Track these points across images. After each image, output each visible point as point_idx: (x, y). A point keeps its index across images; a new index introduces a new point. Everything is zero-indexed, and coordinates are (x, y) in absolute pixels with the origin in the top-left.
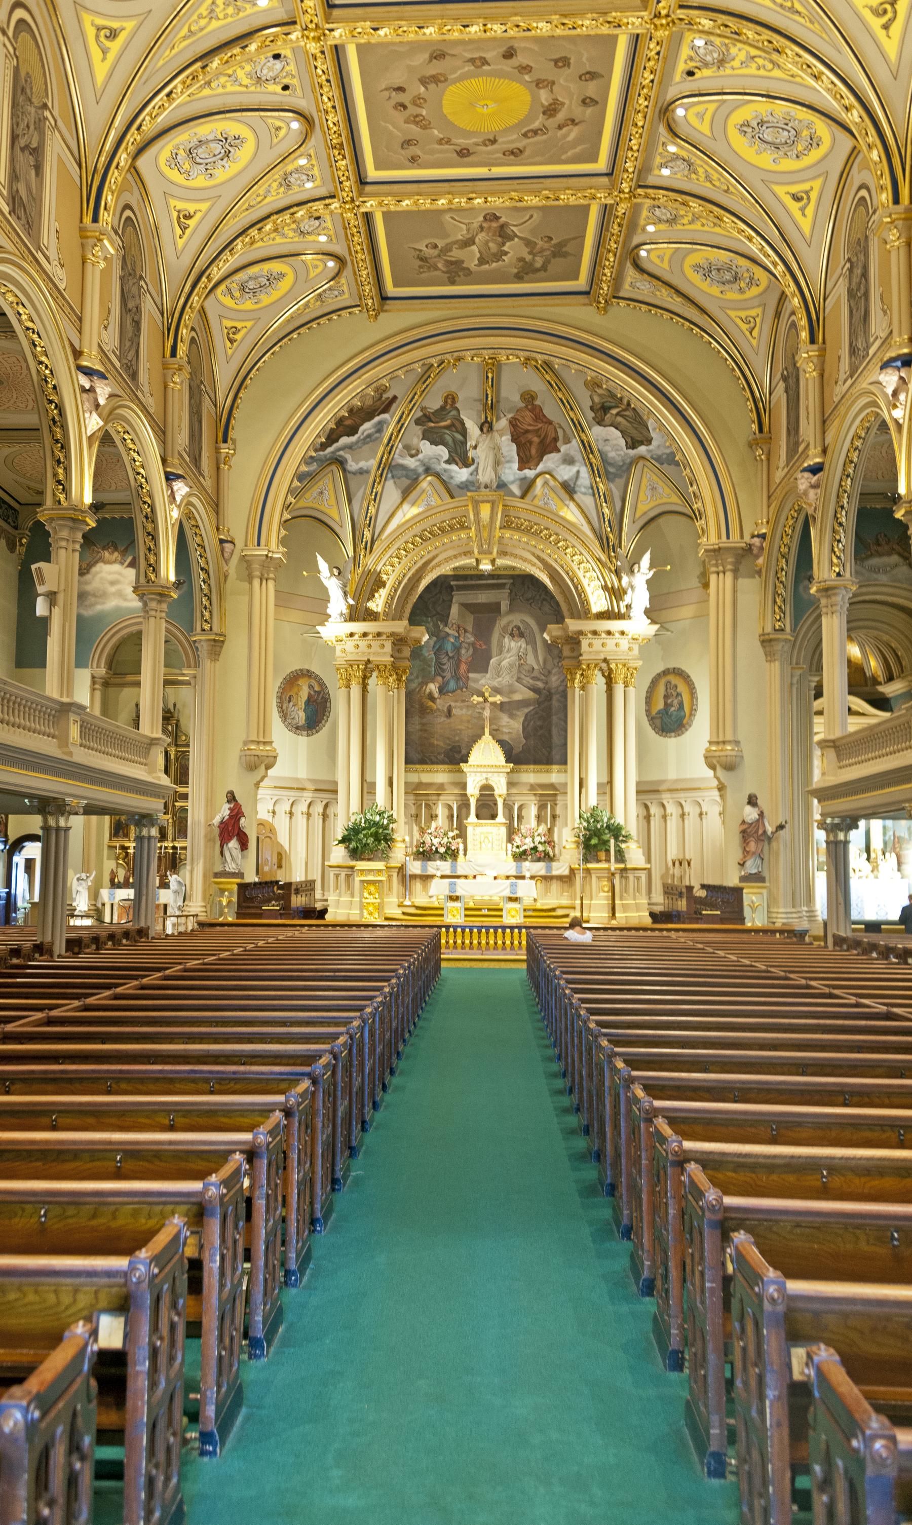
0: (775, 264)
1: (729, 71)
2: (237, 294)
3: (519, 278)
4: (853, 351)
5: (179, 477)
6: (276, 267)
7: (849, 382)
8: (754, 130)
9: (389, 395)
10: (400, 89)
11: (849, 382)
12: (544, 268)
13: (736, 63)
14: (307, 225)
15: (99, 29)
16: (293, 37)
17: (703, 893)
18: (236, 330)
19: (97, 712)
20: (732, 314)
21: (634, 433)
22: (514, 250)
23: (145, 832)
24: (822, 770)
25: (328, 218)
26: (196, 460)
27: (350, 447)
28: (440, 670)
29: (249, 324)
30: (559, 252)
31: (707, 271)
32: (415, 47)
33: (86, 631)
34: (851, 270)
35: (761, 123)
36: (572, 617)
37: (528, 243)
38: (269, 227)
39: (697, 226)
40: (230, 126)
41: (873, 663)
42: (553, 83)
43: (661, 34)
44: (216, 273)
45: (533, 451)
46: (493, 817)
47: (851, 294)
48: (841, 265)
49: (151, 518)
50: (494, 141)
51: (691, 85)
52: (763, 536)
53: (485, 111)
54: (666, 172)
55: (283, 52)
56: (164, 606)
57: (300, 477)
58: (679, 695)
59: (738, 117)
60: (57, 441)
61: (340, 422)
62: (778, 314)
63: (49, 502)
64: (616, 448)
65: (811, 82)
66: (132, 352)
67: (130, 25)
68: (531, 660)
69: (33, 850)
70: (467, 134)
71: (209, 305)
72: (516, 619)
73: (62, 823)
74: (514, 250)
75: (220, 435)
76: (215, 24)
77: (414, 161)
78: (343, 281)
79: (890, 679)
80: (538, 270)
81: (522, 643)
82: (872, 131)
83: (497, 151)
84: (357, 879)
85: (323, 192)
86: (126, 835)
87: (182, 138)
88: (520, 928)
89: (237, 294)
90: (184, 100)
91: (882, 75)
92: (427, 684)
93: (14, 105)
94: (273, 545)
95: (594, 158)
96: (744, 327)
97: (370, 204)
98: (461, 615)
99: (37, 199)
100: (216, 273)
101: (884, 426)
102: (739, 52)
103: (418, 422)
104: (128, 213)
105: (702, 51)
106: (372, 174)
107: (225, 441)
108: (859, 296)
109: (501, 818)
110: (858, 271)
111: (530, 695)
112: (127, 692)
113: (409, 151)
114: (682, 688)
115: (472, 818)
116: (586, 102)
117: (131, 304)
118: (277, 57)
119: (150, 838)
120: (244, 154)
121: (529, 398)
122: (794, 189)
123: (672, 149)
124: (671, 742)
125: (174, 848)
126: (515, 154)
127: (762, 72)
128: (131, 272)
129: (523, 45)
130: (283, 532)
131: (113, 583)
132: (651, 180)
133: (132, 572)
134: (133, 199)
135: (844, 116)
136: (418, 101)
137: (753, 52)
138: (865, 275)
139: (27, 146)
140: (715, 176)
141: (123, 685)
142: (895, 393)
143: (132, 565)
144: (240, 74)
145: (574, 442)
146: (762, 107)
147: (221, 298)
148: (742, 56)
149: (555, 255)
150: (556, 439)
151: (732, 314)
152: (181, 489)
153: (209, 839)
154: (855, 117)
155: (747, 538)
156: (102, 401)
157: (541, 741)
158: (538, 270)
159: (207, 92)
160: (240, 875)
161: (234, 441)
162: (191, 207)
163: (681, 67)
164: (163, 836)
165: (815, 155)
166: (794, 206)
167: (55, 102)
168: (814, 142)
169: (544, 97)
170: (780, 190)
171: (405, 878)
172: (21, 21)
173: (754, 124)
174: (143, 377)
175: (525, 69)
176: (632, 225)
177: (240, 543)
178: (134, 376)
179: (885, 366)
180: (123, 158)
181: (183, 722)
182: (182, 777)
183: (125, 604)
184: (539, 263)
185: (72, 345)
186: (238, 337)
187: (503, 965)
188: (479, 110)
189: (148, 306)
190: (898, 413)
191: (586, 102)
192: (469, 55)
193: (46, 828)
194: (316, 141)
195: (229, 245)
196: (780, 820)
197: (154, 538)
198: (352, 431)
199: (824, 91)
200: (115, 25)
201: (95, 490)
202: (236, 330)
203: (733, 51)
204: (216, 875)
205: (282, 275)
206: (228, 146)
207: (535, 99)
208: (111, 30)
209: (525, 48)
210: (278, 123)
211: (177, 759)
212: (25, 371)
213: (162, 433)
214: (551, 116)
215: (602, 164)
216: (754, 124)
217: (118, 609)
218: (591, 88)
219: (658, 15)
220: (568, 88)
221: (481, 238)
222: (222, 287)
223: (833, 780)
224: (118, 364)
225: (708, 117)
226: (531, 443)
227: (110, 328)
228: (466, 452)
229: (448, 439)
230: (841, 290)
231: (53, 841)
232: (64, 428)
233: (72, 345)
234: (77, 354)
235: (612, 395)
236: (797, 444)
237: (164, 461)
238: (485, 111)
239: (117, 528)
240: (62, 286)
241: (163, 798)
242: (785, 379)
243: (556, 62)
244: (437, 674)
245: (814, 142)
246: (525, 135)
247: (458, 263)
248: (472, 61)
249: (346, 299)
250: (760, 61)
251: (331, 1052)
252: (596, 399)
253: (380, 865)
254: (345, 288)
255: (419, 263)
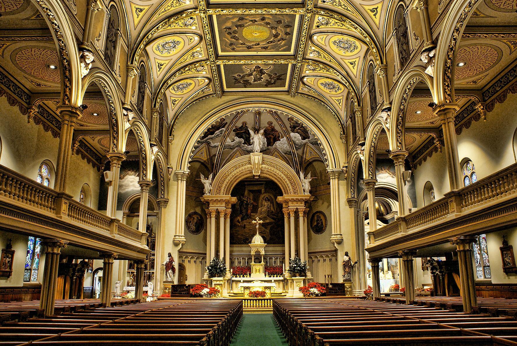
0: (346, 83)
1: (329, 26)
2: (176, 89)
3: (266, 86)
4: (372, 108)
5: (155, 145)
6: (189, 81)
7: (371, 117)
8: (337, 43)
9: (225, 122)
10: (230, 28)
11: (371, 117)
12: (274, 83)
13: (332, 24)
14: (200, 68)
15: (137, 9)
16: (197, 12)
17: (330, 286)
18: (176, 101)
19: (125, 223)
20: (334, 98)
21: (304, 135)
22: (264, 77)
23: (139, 266)
24: (369, 243)
25: (206, 66)
26: (161, 141)
27: (212, 138)
28: (241, 212)
29: (180, 99)
30: (279, 78)
31: (325, 85)
32: (235, 16)
33: (121, 200)
34: (369, 84)
35: (340, 42)
36: (285, 193)
37: (269, 75)
38: (187, 69)
39: (322, 71)
40: (176, 38)
41: (382, 208)
42: (277, 28)
43: (309, 15)
44: (170, 82)
45: (272, 141)
46: (260, 262)
47: (370, 91)
48: (366, 83)
49: (145, 158)
50: (259, 44)
51: (318, 30)
52: (346, 167)
53: (256, 35)
54: (311, 55)
55: (193, 17)
56: (148, 188)
57: (196, 148)
58: (321, 220)
59: (333, 40)
60: (115, 131)
61: (209, 130)
62: (347, 99)
63: (111, 151)
64: (298, 140)
65: (354, 30)
66: (141, 105)
67: (146, 8)
68: (272, 208)
69: (100, 274)
70: (249, 42)
71: (167, 92)
72: (267, 195)
73: (111, 261)
74: (264, 77)
75: (169, 133)
76: (173, 8)
77: (233, 50)
78: (210, 86)
79: (388, 213)
80: (273, 84)
81: (269, 203)
82: (373, 43)
83: (260, 47)
84: (213, 283)
85: (205, 58)
86: (133, 268)
87: (160, 41)
88: (270, 299)
89: (176, 89)
90: (161, 31)
91: (375, 28)
92: (237, 217)
93: (108, 28)
94: (186, 170)
95: (289, 50)
96: (337, 102)
97: (219, 62)
98: (249, 194)
99: (113, 56)
100: (170, 82)
101: (383, 131)
102: (332, 21)
103: (234, 131)
104: (142, 63)
105: (321, 21)
106: (220, 53)
107: (170, 135)
108: (372, 91)
109: (262, 263)
110: (372, 84)
111: (272, 220)
112: (135, 218)
113: (232, 46)
114: (322, 217)
115: (253, 263)
116: (287, 34)
117: (142, 90)
118: (191, 18)
119: (141, 268)
120: (179, 47)
121: (270, 123)
122: (350, 61)
123: (313, 48)
124: (319, 236)
125: (150, 273)
126: (265, 48)
127: (339, 27)
128: (143, 79)
129: (267, 16)
130: (189, 165)
131: (131, 182)
132: (307, 57)
133: (138, 178)
134: (145, 59)
135: (365, 40)
136: (235, 32)
137: (337, 21)
138: (374, 85)
139: (111, 40)
140: (327, 57)
141: (133, 217)
142: (386, 120)
143: (139, 175)
144: (180, 23)
145: (285, 138)
146: (340, 37)
147: (171, 91)
148: (333, 22)
149: (278, 79)
150: (279, 137)
151: (334, 98)
152: (155, 149)
153: (162, 269)
154: (368, 39)
155: (341, 167)
156: (130, 119)
157: (275, 235)
158: (273, 84)
159: (169, 28)
160: (173, 282)
161: (174, 136)
162: (162, 62)
163: (315, 24)
164: (146, 269)
165: (356, 51)
166: (351, 66)
167: (121, 29)
168: (356, 47)
169: (274, 32)
170: (346, 61)
171: (230, 282)
172: (112, 5)
173: (338, 42)
174: (145, 113)
175: (268, 24)
176: (301, 70)
177: (174, 168)
178: (141, 112)
179: (383, 111)
180: (142, 46)
181: (154, 229)
182: (153, 247)
183: (135, 189)
184: (273, 81)
185: (121, 101)
186: (176, 103)
187: (264, 313)
188: (254, 35)
189: (148, 91)
190: (388, 125)
191: (287, 34)
192: (251, 19)
193: (105, 263)
194: (203, 43)
195: (174, 74)
196: (356, 260)
197: (146, 165)
198: (212, 133)
199: (357, 32)
200: (142, 8)
201: (127, 145)
202: (176, 101)
203: (331, 21)
204: (164, 282)
205: (191, 84)
206: (175, 44)
207: (271, 32)
208: (141, 9)
209: (268, 18)
210: (191, 38)
211: (151, 242)
212: (106, 111)
213: (150, 131)
214: (277, 37)
215: (292, 52)
216: (338, 42)
217: (133, 190)
218: (288, 30)
219: (308, 9)
220: (281, 30)
221: (254, 73)
222: (171, 87)
223: (372, 245)
224: (136, 108)
225: (324, 39)
226: (271, 138)
227: (135, 97)
228: (250, 140)
229: (244, 136)
230: (367, 90)
231: (107, 269)
232: (117, 127)
233: (121, 101)
234: (123, 104)
235: (297, 123)
236: (356, 138)
237: (150, 140)
238: (256, 35)
239: (133, 163)
240: (120, 83)
241: (146, 254)
242: (351, 118)
243: (277, 22)
244: (240, 214)
245: (356, 47)
246: (268, 43)
247: (247, 81)
248: (252, 21)
249: (211, 92)
250: (339, 24)
251: (207, 336)
252: (292, 124)
253: (221, 278)
254: (211, 88)
255: (234, 81)
